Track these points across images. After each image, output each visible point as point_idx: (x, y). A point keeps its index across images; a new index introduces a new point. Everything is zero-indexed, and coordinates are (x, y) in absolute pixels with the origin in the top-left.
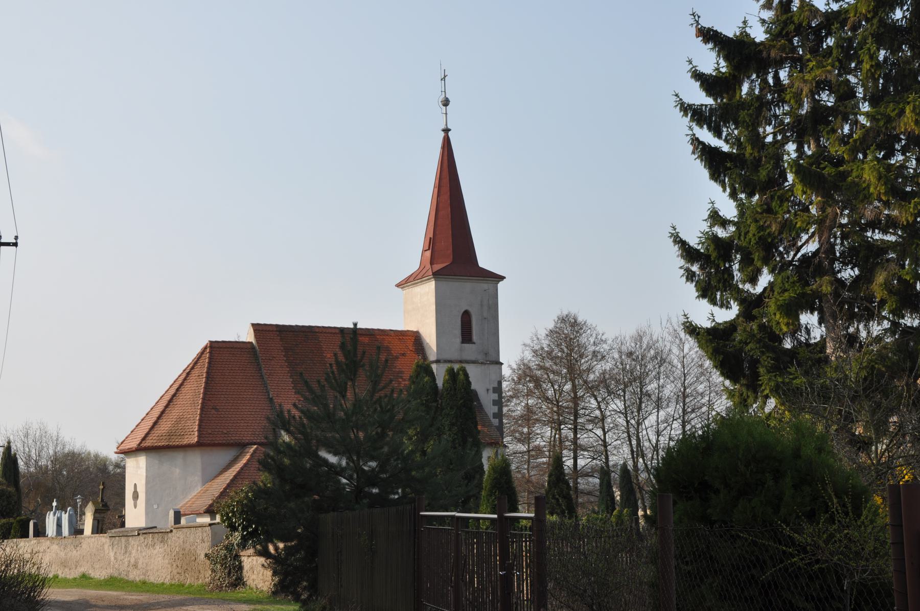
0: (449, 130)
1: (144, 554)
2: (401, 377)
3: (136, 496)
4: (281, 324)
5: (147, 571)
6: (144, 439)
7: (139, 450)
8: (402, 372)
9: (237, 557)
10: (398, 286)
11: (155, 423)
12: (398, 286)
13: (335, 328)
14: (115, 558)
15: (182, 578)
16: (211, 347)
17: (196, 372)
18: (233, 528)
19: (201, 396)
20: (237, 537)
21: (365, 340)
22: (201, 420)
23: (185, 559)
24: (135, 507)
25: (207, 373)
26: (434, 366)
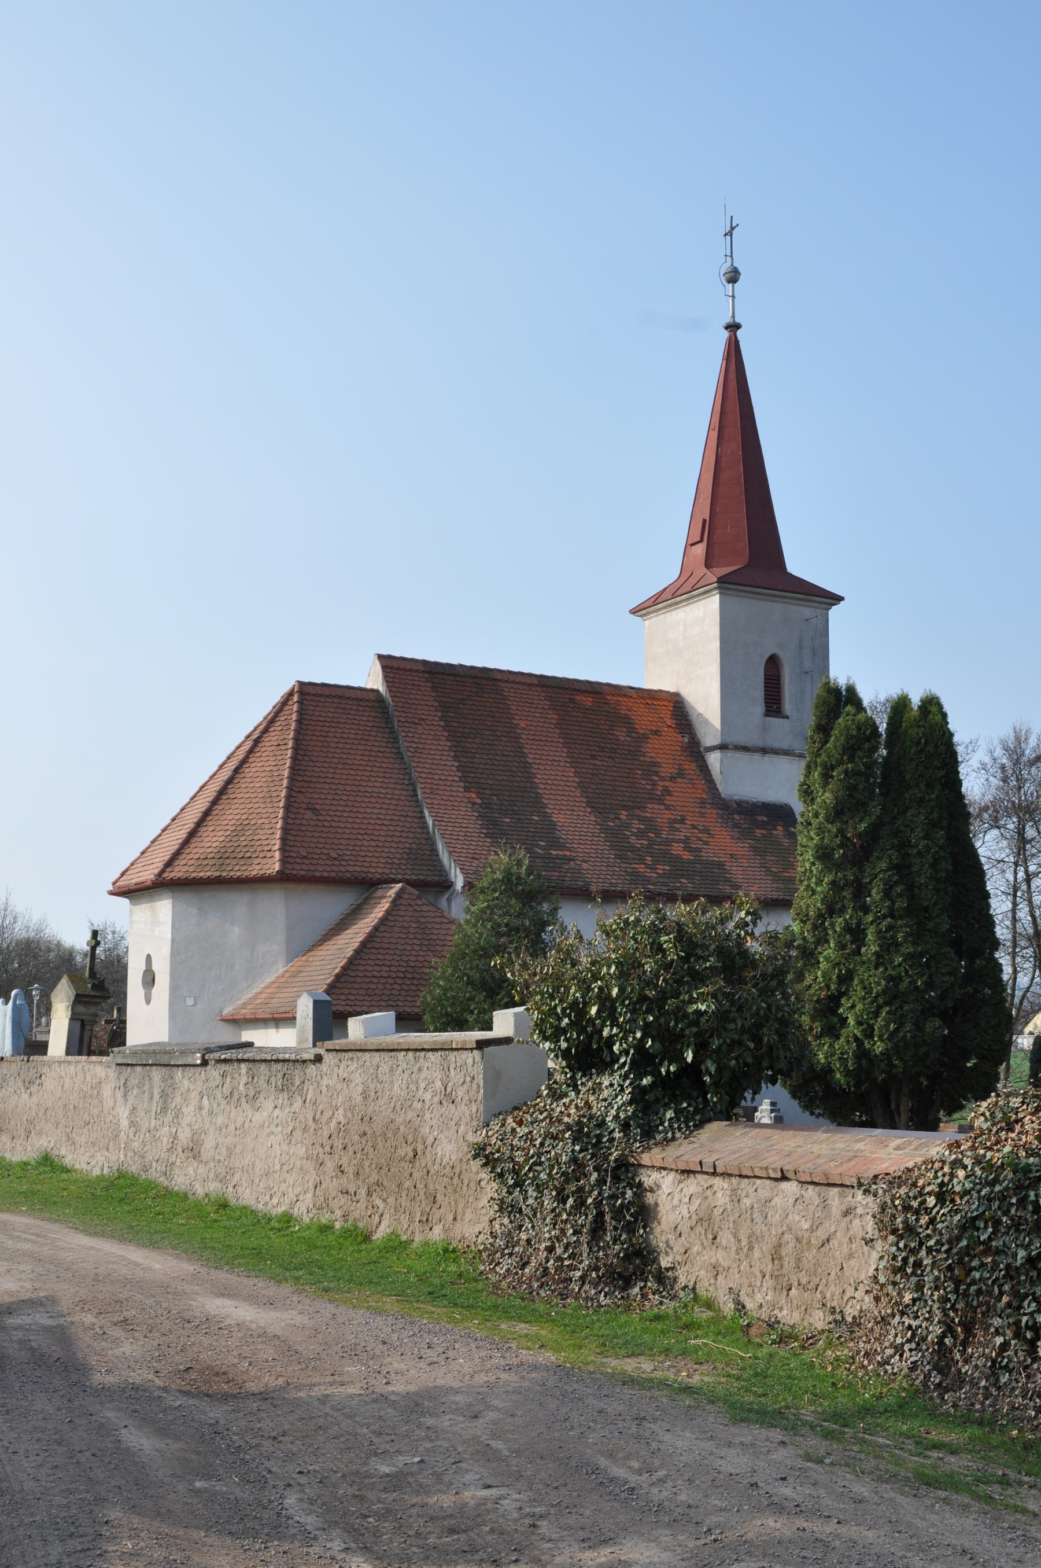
0: (738, 326)
1: (220, 1120)
2: (657, 774)
3: (149, 979)
4: (432, 659)
5: (231, 1171)
6: (169, 864)
7: (162, 885)
8: (655, 764)
9: (625, 1171)
10: (634, 612)
11: (192, 834)
12: (634, 612)
13: (530, 675)
14: (132, 1124)
15: (359, 1210)
16: (301, 692)
17: (272, 737)
18: (588, 1058)
19: (285, 783)
20: (610, 1094)
21: (587, 701)
22: (285, 830)
23: (379, 1150)
24: (148, 1001)
25: (296, 739)
26: (714, 760)
